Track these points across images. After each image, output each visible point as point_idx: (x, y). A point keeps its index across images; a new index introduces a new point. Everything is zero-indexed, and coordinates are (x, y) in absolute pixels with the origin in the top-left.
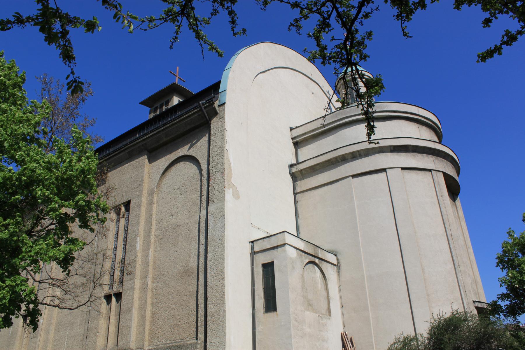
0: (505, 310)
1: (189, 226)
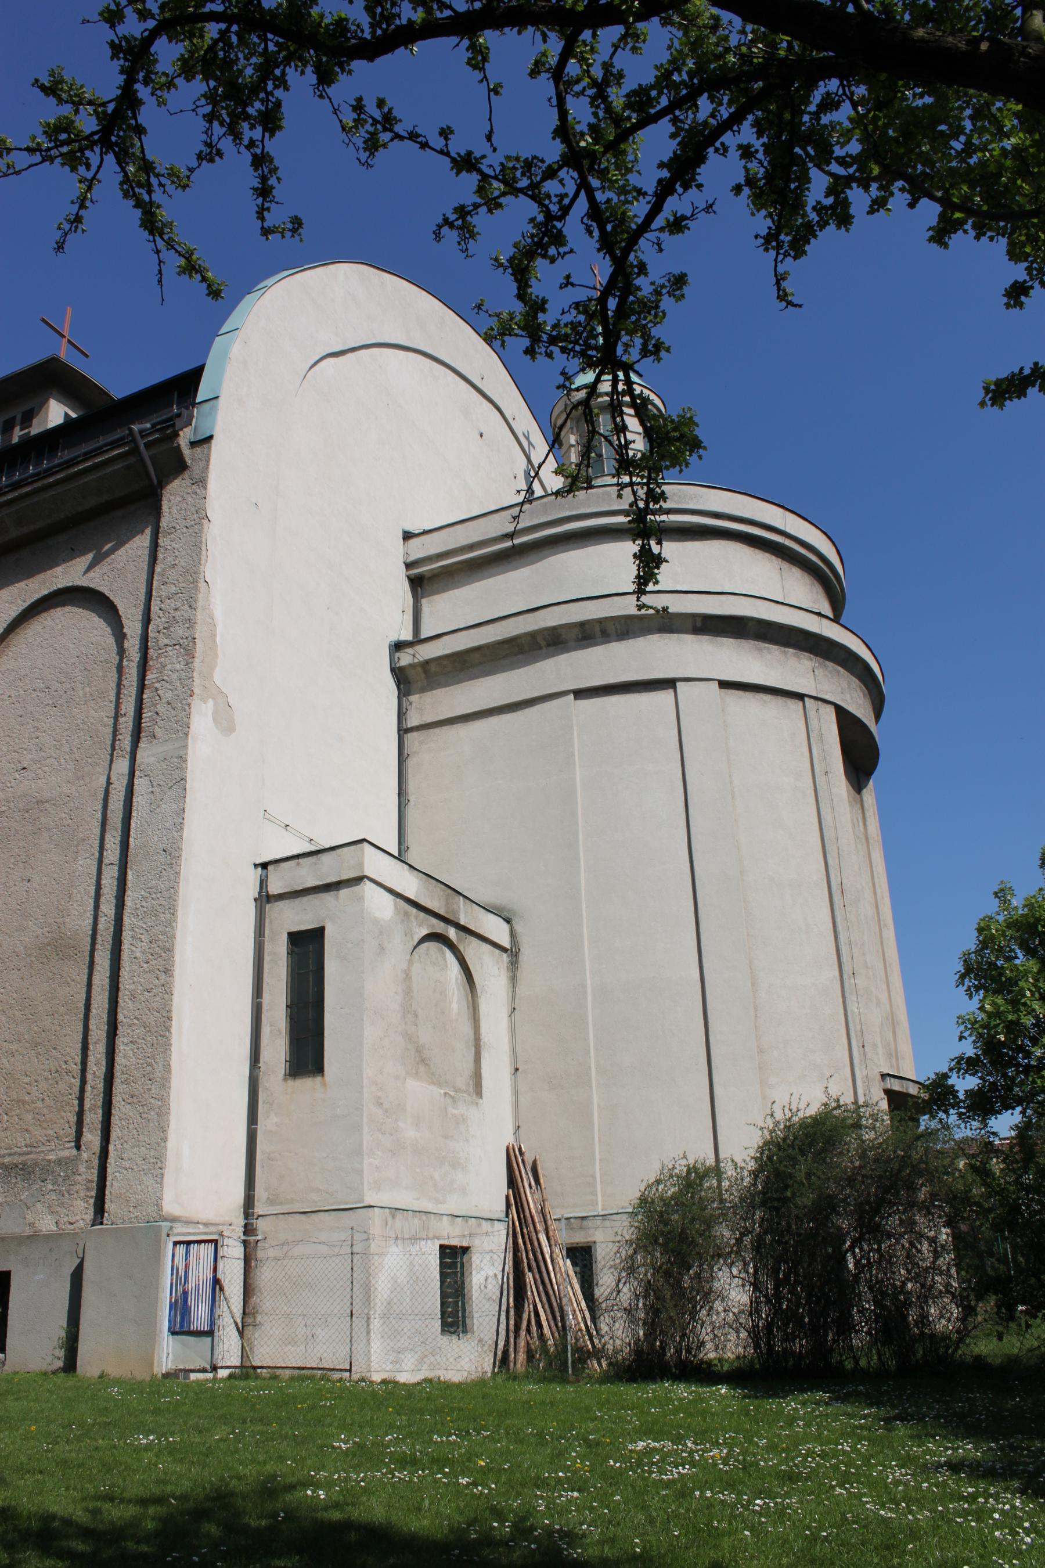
0: (964, 1102)
1: (72, 805)
